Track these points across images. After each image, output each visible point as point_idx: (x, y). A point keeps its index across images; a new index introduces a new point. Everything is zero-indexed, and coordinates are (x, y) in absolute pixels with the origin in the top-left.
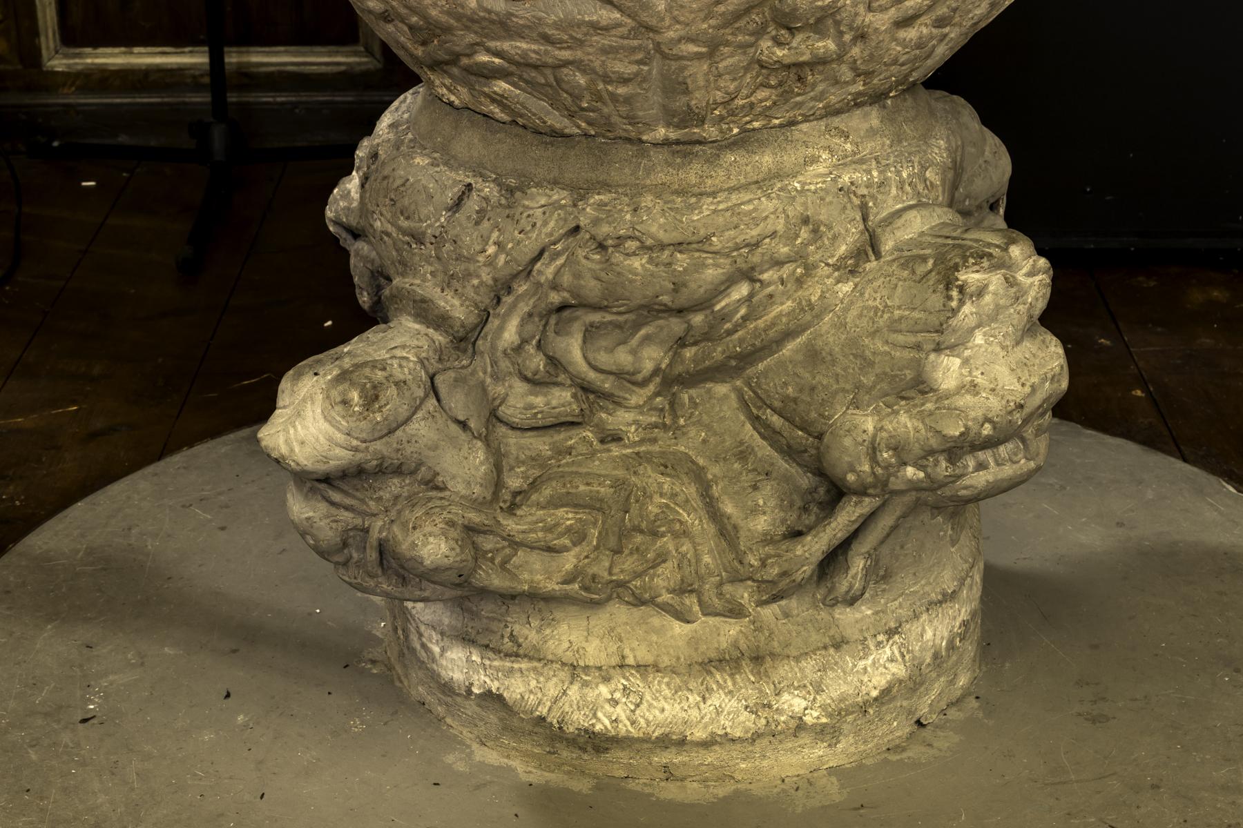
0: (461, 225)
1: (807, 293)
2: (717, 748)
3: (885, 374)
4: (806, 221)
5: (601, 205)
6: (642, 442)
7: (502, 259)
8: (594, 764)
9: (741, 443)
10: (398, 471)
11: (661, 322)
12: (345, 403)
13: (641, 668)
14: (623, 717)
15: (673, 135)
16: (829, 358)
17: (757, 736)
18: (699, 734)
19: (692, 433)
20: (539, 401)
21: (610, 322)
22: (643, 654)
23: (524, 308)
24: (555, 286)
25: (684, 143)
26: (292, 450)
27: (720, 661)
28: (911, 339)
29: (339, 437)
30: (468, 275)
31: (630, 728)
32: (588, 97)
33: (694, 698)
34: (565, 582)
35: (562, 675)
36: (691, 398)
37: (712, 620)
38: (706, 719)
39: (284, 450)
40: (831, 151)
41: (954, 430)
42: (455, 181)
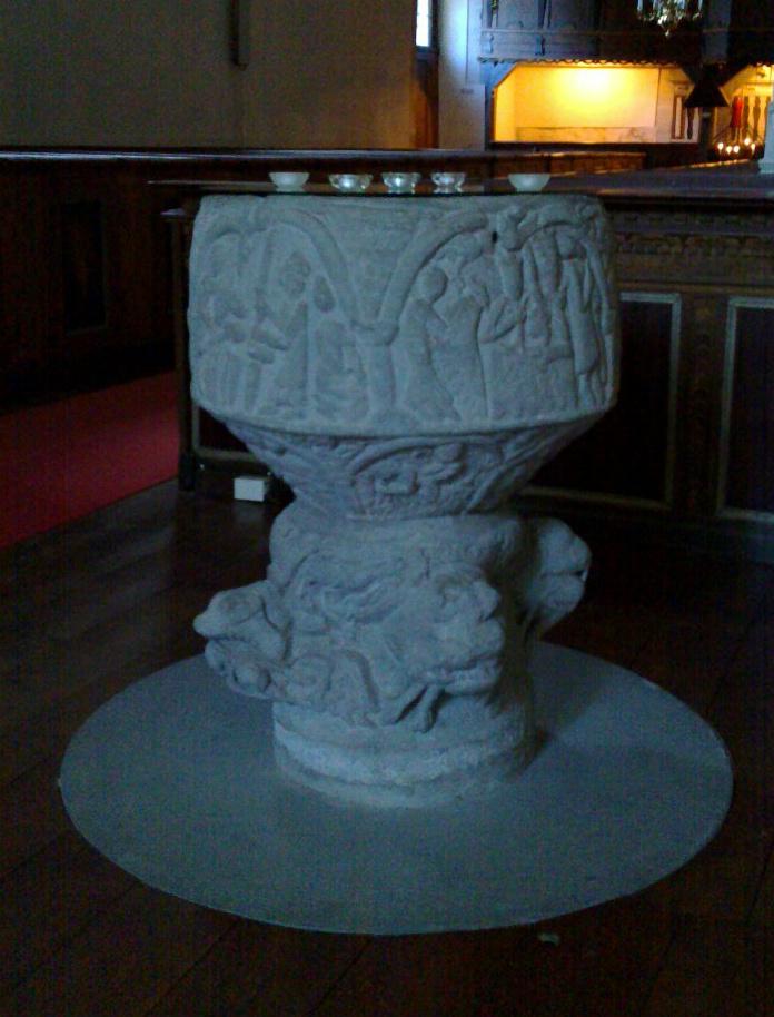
10: (242, 639)
18: (349, 779)
23: (303, 581)
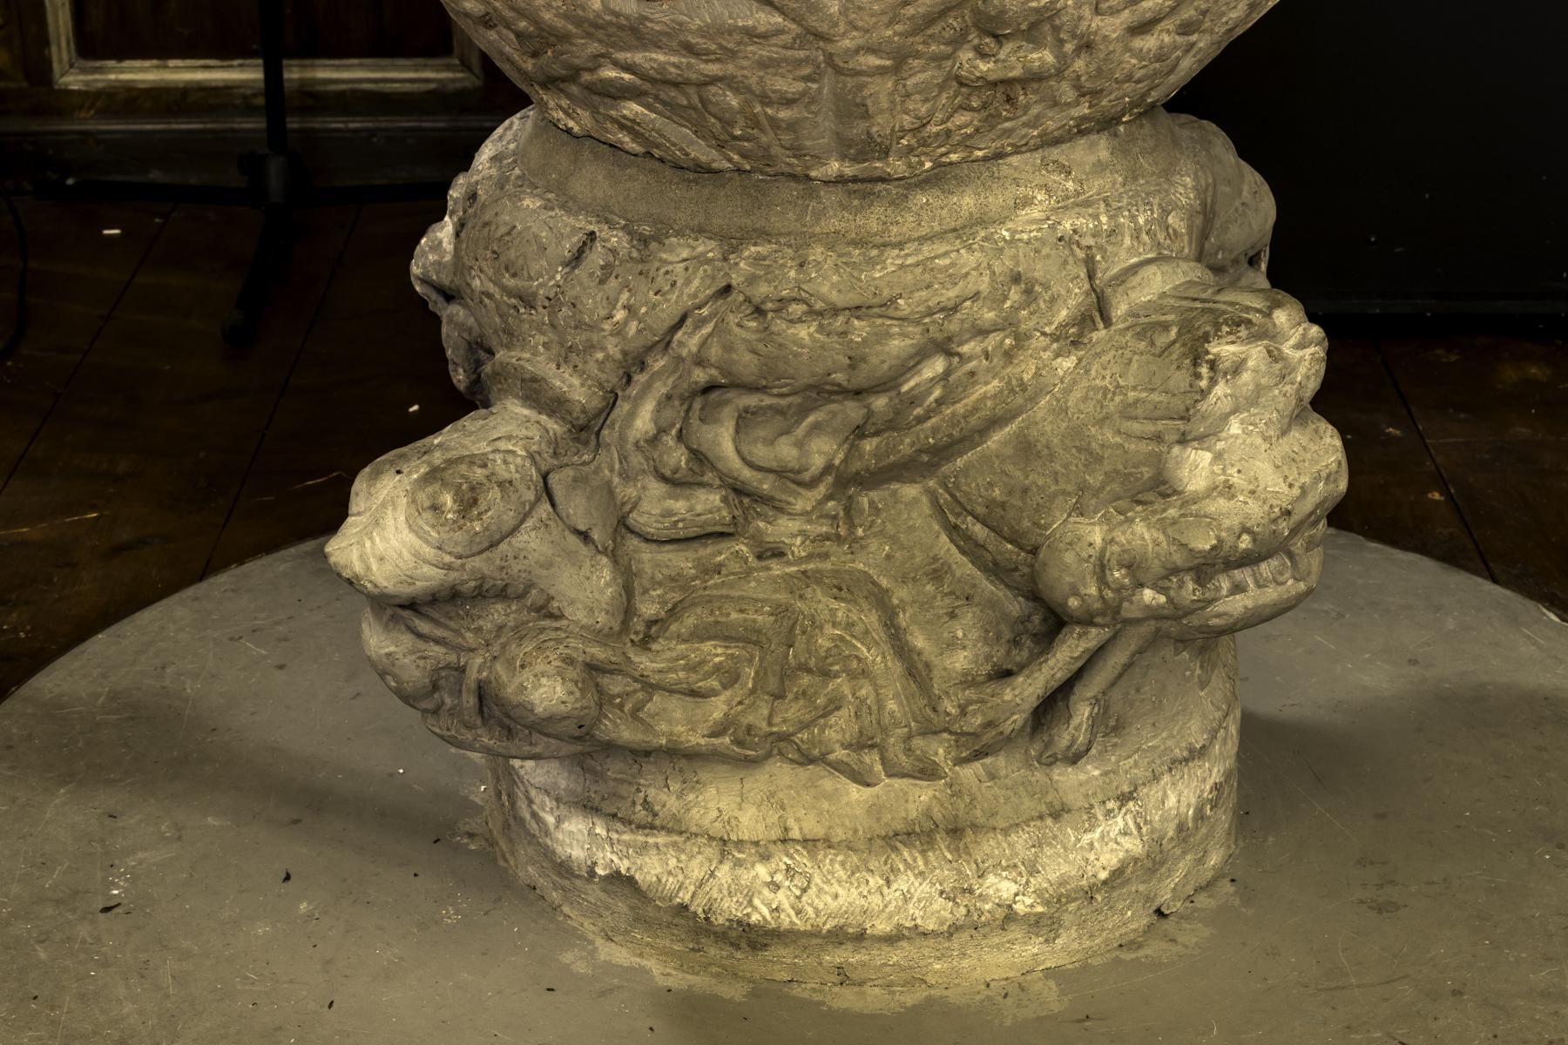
0: (581, 284)
1: (1018, 370)
2: (904, 944)
3: (1117, 472)
4: (1016, 279)
5: (759, 258)
6: (810, 557)
7: (633, 327)
8: (750, 964)
9: (935, 559)
10: (502, 594)
11: (834, 406)
12: (436, 508)
13: (809, 843)
14: (786, 905)
15: (849, 171)
16: (1046, 451)
17: (954, 929)
18: (882, 927)
19: (873, 547)
20: (680, 506)
21: (770, 407)
22: (811, 826)
23: (661, 389)
24: (700, 361)
25: (863, 181)
26: (368, 568)
27: (909, 834)
28: (1150, 428)
29: (428, 551)
30: (591, 347)
31: (795, 919)
32: (741, 122)
33: (875, 881)
34: (713, 735)
35: (709, 851)
36: (871, 503)
37: (898, 783)
38: (891, 908)
39: (358, 568)
40: (1048, 191)
41: (1204, 543)
42: (573, 228)
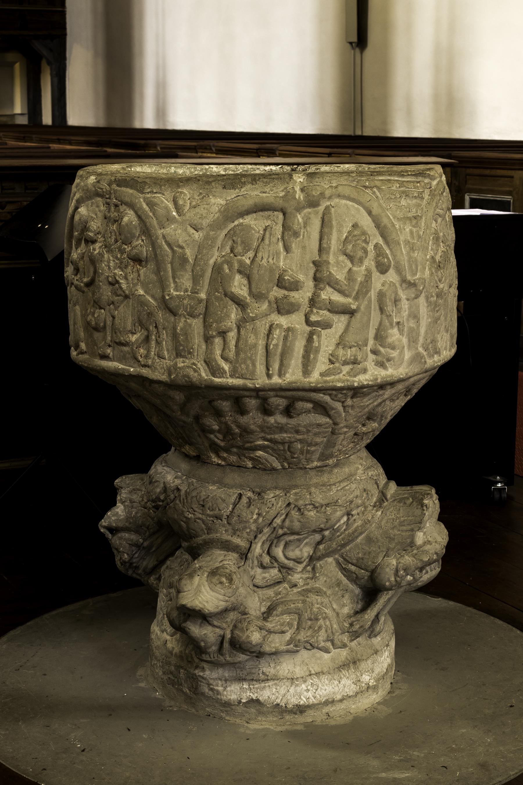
0: (240, 509)
1: (366, 517)
2: (345, 701)
3: (399, 542)
4: (365, 490)
5: (296, 494)
6: (304, 585)
7: (261, 519)
8: (301, 719)
9: (338, 579)
11: (312, 537)
12: (221, 583)
13: (317, 674)
14: (311, 696)
16: (376, 540)
17: (357, 693)
18: (339, 697)
19: (321, 579)
20: (267, 575)
21: (297, 539)
22: (317, 669)
24: (282, 527)
25: (322, 467)
26: (204, 605)
27: (344, 665)
28: (409, 528)
29: (221, 597)
30: (245, 528)
31: (314, 700)
33: (336, 682)
34: (288, 645)
35: (287, 684)
36: (320, 565)
37: (337, 650)
38: (341, 690)
39: (201, 606)
40: (362, 465)
41: (426, 559)
42: (234, 493)
